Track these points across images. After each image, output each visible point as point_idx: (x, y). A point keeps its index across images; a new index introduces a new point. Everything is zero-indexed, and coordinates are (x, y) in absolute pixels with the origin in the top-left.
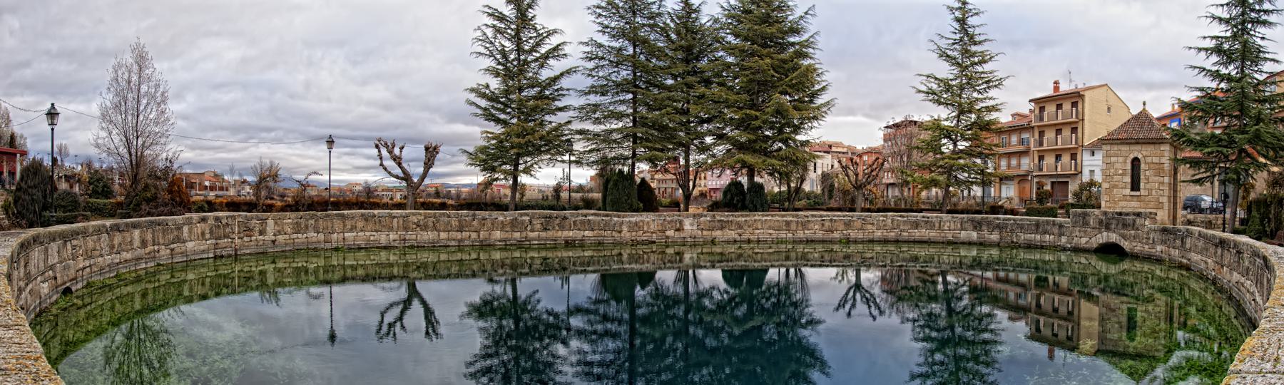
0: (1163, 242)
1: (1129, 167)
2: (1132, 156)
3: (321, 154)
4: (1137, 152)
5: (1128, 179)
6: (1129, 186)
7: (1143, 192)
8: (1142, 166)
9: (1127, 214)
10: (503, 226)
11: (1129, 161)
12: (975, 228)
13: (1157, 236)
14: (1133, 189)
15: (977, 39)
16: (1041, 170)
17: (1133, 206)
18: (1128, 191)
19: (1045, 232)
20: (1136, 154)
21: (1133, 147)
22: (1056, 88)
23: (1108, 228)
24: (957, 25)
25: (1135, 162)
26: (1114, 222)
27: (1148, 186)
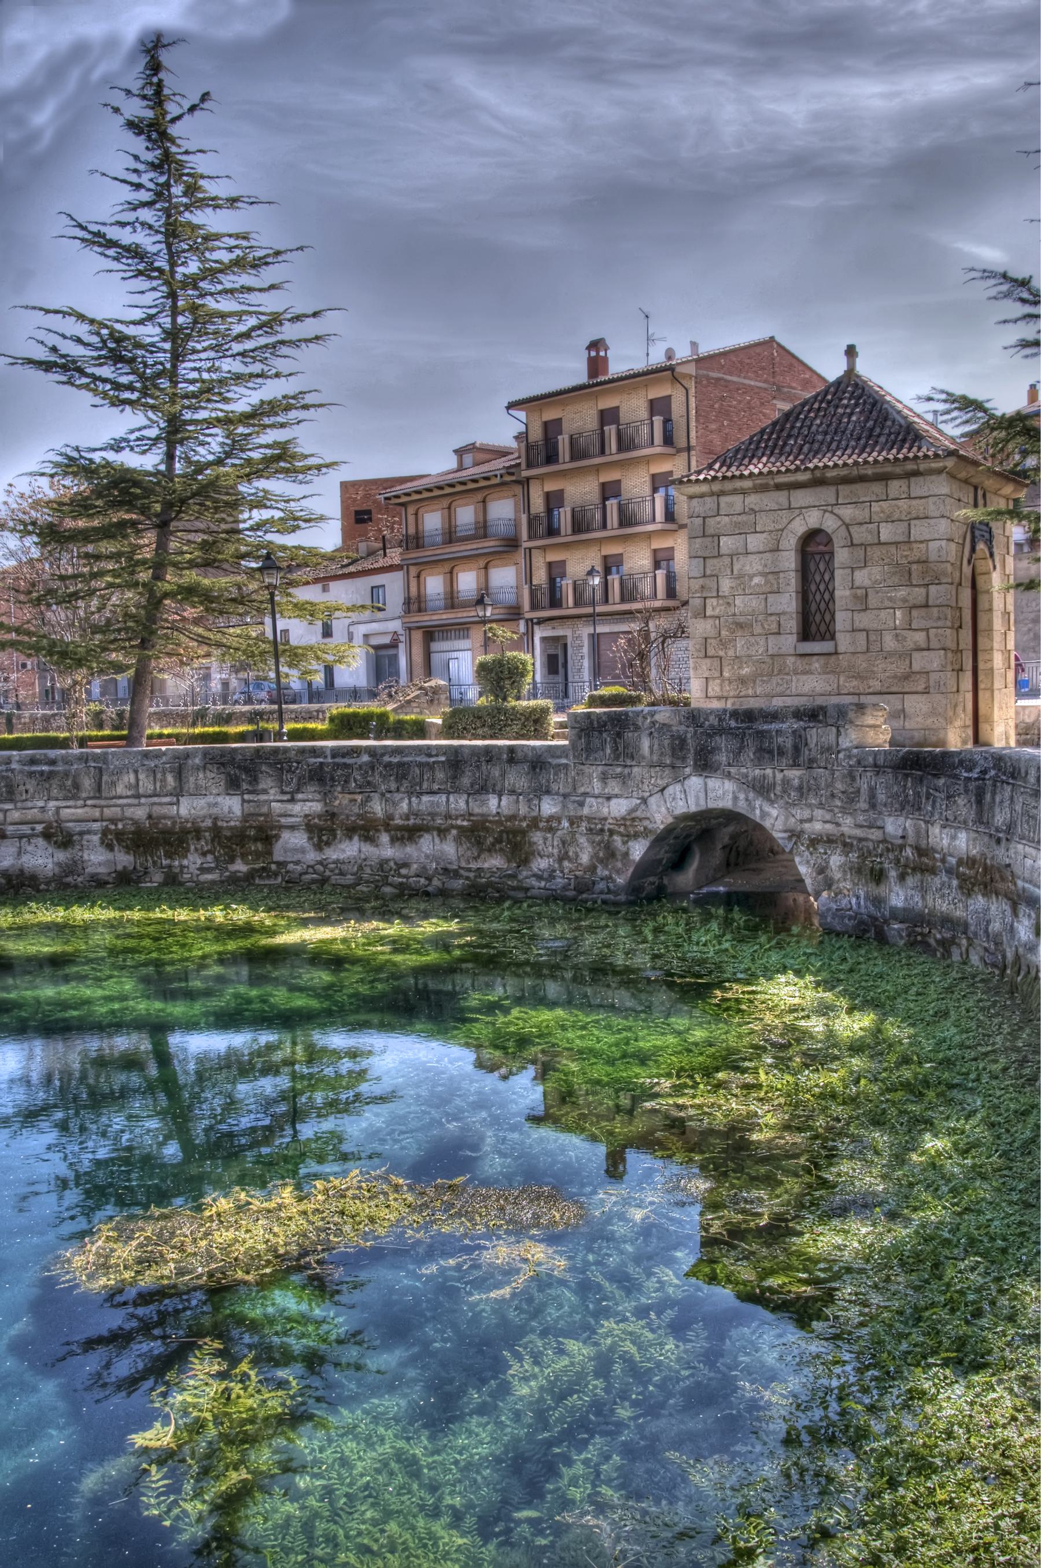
0: (905, 806)
1: (789, 560)
2: (799, 527)
3: (692, 801)
4: (811, 513)
5: (788, 602)
6: (792, 624)
7: (843, 641)
8: (842, 556)
9: (774, 716)
10: (923, 863)
11: (790, 542)
12: (233, 785)
13: (884, 787)
14: (806, 634)
15: (211, 188)
16: (555, 602)
17: (811, 685)
18: (789, 641)
19: (482, 788)
20: (813, 519)
21: (801, 497)
22: (596, 366)
23: (705, 765)
24: (139, 144)
25: (814, 548)
26: (721, 741)
27: (864, 620)
